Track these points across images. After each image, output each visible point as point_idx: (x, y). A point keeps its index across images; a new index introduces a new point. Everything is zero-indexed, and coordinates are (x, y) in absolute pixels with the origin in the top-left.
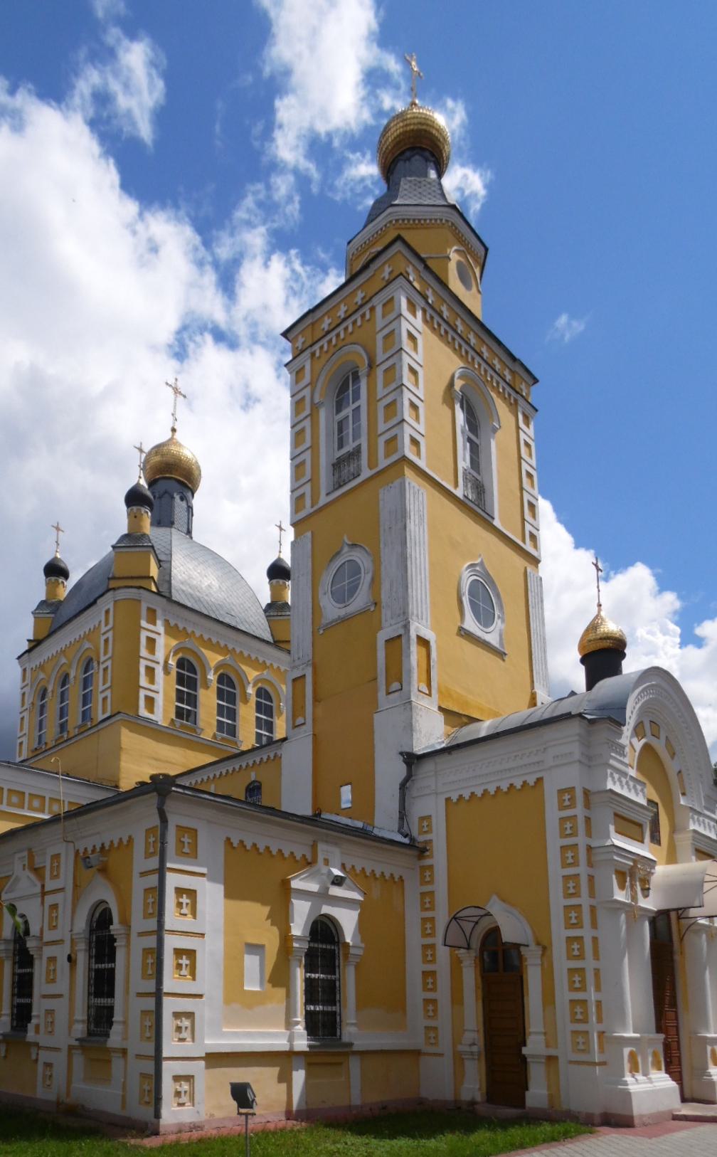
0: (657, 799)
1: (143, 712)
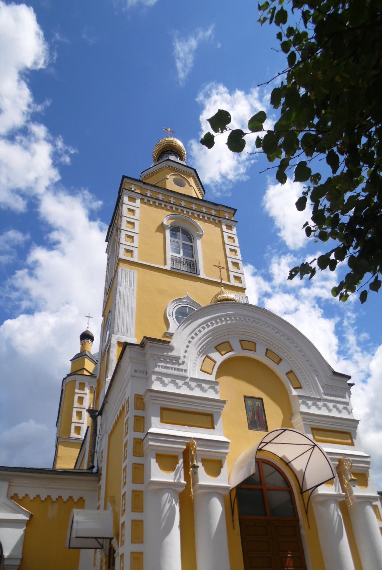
0: (256, 392)
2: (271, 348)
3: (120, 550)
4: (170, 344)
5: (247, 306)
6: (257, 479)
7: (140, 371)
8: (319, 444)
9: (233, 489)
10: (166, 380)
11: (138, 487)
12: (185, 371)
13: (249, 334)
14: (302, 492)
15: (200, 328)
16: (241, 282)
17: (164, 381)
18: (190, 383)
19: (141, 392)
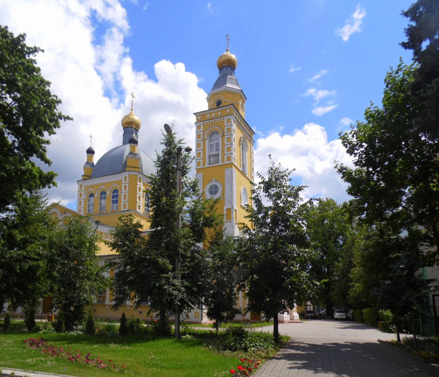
1: (138, 210)
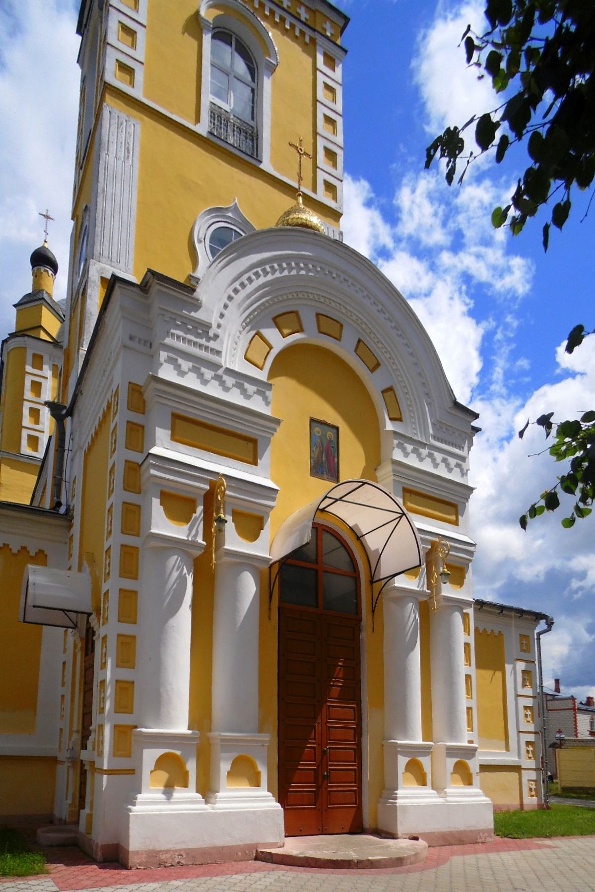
0: (331, 416)
2: (366, 340)
3: (101, 631)
4: (195, 295)
5: (339, 246)
6: (311, 552)
7: (140, 340)
8: (411, 515)
9: (275, 563)
10: (185, 365)
11: (130, 540)
12: (219, 353)
13: (333, 305)
14: (372, 582)
15: (251, 274)
16: (335, 198)
17: (180, 366)
18: (225, 378)
19: (140, 381)
